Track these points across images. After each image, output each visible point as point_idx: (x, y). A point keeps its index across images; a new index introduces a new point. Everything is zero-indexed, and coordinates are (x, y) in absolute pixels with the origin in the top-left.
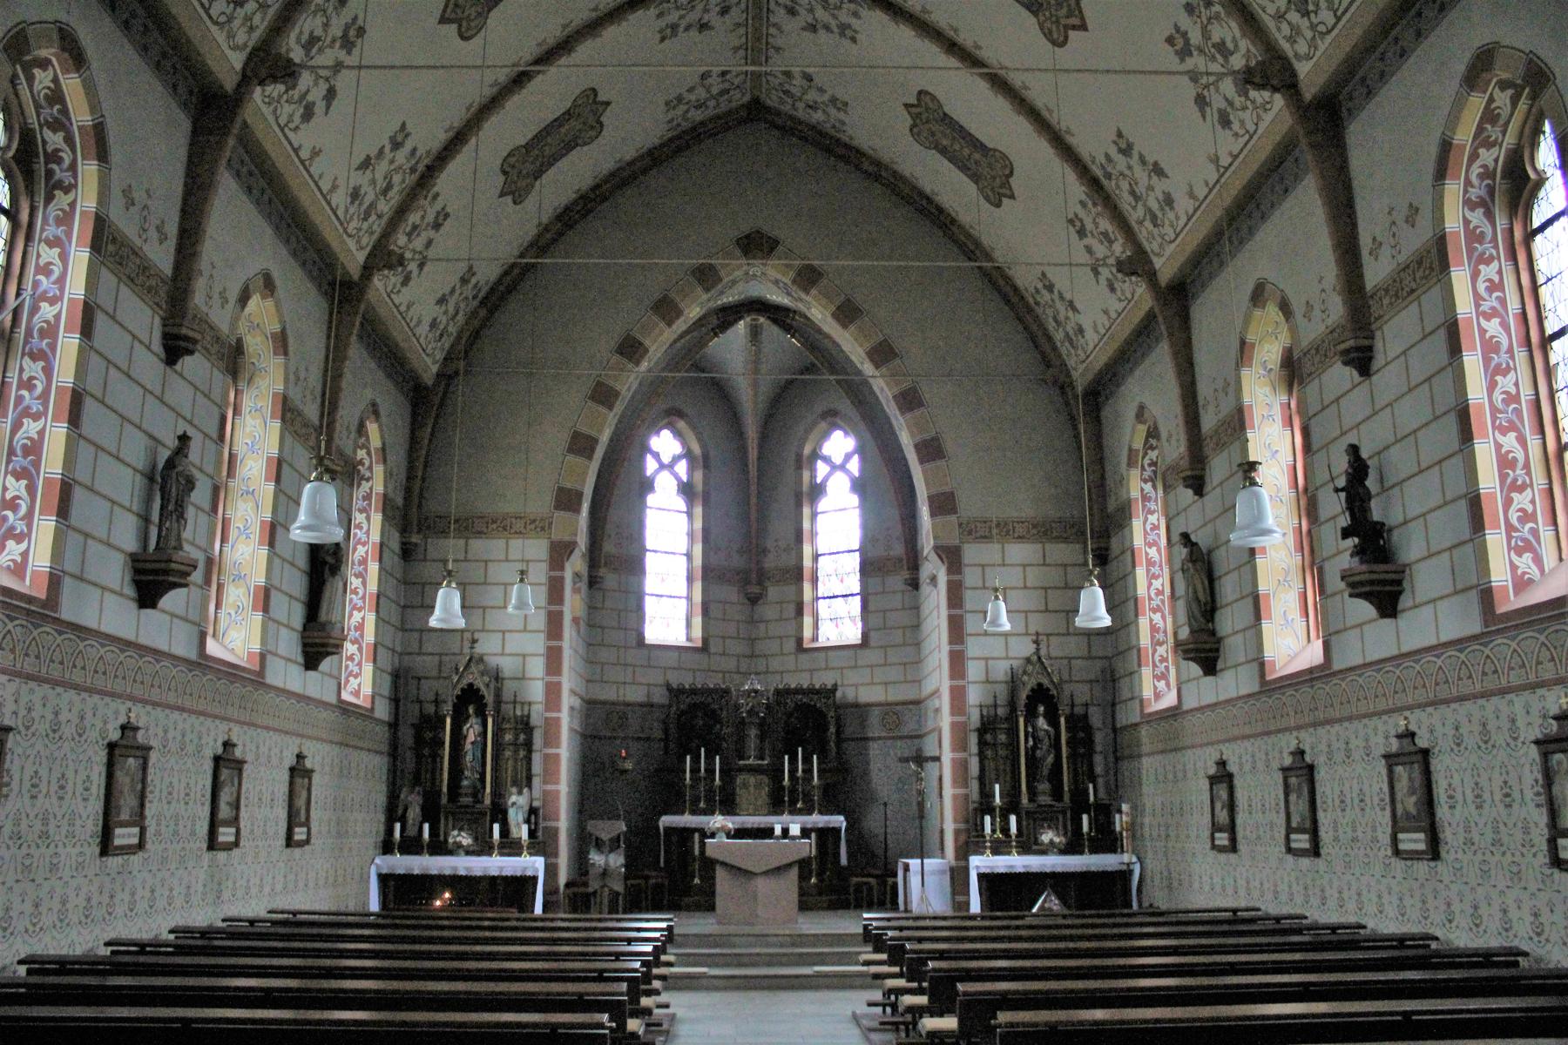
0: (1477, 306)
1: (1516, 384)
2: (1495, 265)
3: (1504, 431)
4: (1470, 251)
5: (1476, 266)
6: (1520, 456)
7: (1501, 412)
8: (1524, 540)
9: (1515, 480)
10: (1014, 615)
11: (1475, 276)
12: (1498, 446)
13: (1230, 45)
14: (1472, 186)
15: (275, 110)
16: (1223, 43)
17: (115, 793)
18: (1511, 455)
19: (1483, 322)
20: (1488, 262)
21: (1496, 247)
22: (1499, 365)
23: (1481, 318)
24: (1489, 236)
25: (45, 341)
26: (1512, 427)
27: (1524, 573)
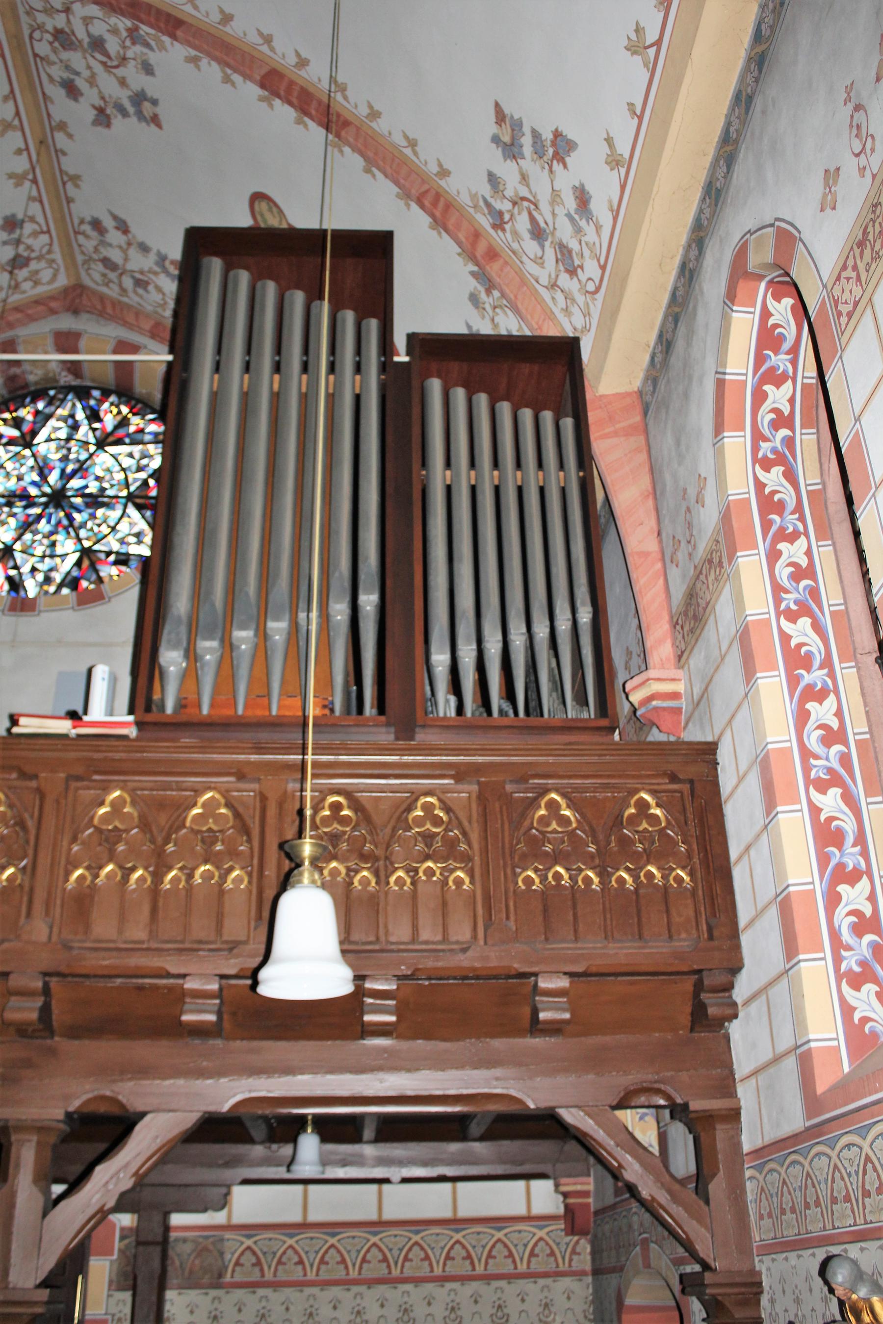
0: (778, 601)
1: (839, 714)
2: (802, 542)
3: (822, 787)
4: (766, 525)
5: (775, 542)
6: (849, 826)
7: (817, 757)
8: (830, 771)
9: (782, 529)
10: (349, 955)
11: (773, 556)
12: (815, 811)
13: (140, 291)
14: (787, 592)
15: (49, 252)
16: (146, 289)
17: (335, 418)
18: (804, 650)
19: (786, 625)
20: (792, 538)
21: (802, 519)
22: (782, 529)
23: (811, 787)
24: (791, 504)
25: (30, 418)
26: (834, 780)
27: (800, 645)
